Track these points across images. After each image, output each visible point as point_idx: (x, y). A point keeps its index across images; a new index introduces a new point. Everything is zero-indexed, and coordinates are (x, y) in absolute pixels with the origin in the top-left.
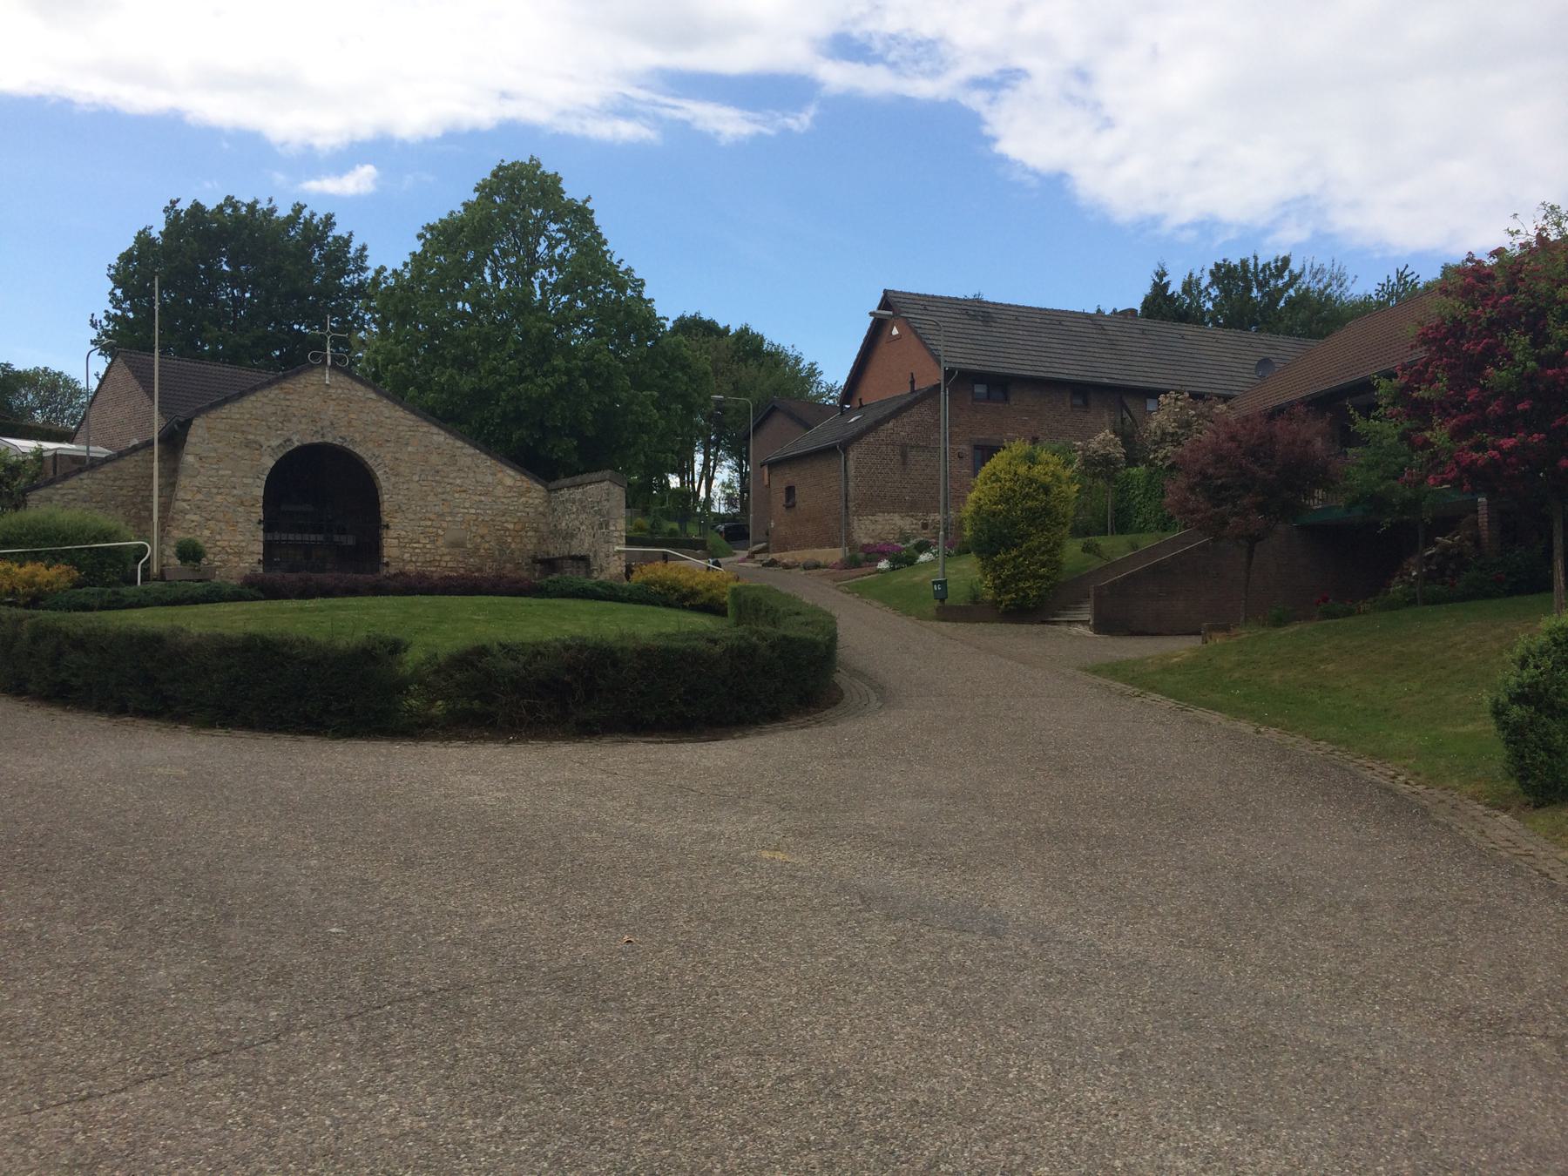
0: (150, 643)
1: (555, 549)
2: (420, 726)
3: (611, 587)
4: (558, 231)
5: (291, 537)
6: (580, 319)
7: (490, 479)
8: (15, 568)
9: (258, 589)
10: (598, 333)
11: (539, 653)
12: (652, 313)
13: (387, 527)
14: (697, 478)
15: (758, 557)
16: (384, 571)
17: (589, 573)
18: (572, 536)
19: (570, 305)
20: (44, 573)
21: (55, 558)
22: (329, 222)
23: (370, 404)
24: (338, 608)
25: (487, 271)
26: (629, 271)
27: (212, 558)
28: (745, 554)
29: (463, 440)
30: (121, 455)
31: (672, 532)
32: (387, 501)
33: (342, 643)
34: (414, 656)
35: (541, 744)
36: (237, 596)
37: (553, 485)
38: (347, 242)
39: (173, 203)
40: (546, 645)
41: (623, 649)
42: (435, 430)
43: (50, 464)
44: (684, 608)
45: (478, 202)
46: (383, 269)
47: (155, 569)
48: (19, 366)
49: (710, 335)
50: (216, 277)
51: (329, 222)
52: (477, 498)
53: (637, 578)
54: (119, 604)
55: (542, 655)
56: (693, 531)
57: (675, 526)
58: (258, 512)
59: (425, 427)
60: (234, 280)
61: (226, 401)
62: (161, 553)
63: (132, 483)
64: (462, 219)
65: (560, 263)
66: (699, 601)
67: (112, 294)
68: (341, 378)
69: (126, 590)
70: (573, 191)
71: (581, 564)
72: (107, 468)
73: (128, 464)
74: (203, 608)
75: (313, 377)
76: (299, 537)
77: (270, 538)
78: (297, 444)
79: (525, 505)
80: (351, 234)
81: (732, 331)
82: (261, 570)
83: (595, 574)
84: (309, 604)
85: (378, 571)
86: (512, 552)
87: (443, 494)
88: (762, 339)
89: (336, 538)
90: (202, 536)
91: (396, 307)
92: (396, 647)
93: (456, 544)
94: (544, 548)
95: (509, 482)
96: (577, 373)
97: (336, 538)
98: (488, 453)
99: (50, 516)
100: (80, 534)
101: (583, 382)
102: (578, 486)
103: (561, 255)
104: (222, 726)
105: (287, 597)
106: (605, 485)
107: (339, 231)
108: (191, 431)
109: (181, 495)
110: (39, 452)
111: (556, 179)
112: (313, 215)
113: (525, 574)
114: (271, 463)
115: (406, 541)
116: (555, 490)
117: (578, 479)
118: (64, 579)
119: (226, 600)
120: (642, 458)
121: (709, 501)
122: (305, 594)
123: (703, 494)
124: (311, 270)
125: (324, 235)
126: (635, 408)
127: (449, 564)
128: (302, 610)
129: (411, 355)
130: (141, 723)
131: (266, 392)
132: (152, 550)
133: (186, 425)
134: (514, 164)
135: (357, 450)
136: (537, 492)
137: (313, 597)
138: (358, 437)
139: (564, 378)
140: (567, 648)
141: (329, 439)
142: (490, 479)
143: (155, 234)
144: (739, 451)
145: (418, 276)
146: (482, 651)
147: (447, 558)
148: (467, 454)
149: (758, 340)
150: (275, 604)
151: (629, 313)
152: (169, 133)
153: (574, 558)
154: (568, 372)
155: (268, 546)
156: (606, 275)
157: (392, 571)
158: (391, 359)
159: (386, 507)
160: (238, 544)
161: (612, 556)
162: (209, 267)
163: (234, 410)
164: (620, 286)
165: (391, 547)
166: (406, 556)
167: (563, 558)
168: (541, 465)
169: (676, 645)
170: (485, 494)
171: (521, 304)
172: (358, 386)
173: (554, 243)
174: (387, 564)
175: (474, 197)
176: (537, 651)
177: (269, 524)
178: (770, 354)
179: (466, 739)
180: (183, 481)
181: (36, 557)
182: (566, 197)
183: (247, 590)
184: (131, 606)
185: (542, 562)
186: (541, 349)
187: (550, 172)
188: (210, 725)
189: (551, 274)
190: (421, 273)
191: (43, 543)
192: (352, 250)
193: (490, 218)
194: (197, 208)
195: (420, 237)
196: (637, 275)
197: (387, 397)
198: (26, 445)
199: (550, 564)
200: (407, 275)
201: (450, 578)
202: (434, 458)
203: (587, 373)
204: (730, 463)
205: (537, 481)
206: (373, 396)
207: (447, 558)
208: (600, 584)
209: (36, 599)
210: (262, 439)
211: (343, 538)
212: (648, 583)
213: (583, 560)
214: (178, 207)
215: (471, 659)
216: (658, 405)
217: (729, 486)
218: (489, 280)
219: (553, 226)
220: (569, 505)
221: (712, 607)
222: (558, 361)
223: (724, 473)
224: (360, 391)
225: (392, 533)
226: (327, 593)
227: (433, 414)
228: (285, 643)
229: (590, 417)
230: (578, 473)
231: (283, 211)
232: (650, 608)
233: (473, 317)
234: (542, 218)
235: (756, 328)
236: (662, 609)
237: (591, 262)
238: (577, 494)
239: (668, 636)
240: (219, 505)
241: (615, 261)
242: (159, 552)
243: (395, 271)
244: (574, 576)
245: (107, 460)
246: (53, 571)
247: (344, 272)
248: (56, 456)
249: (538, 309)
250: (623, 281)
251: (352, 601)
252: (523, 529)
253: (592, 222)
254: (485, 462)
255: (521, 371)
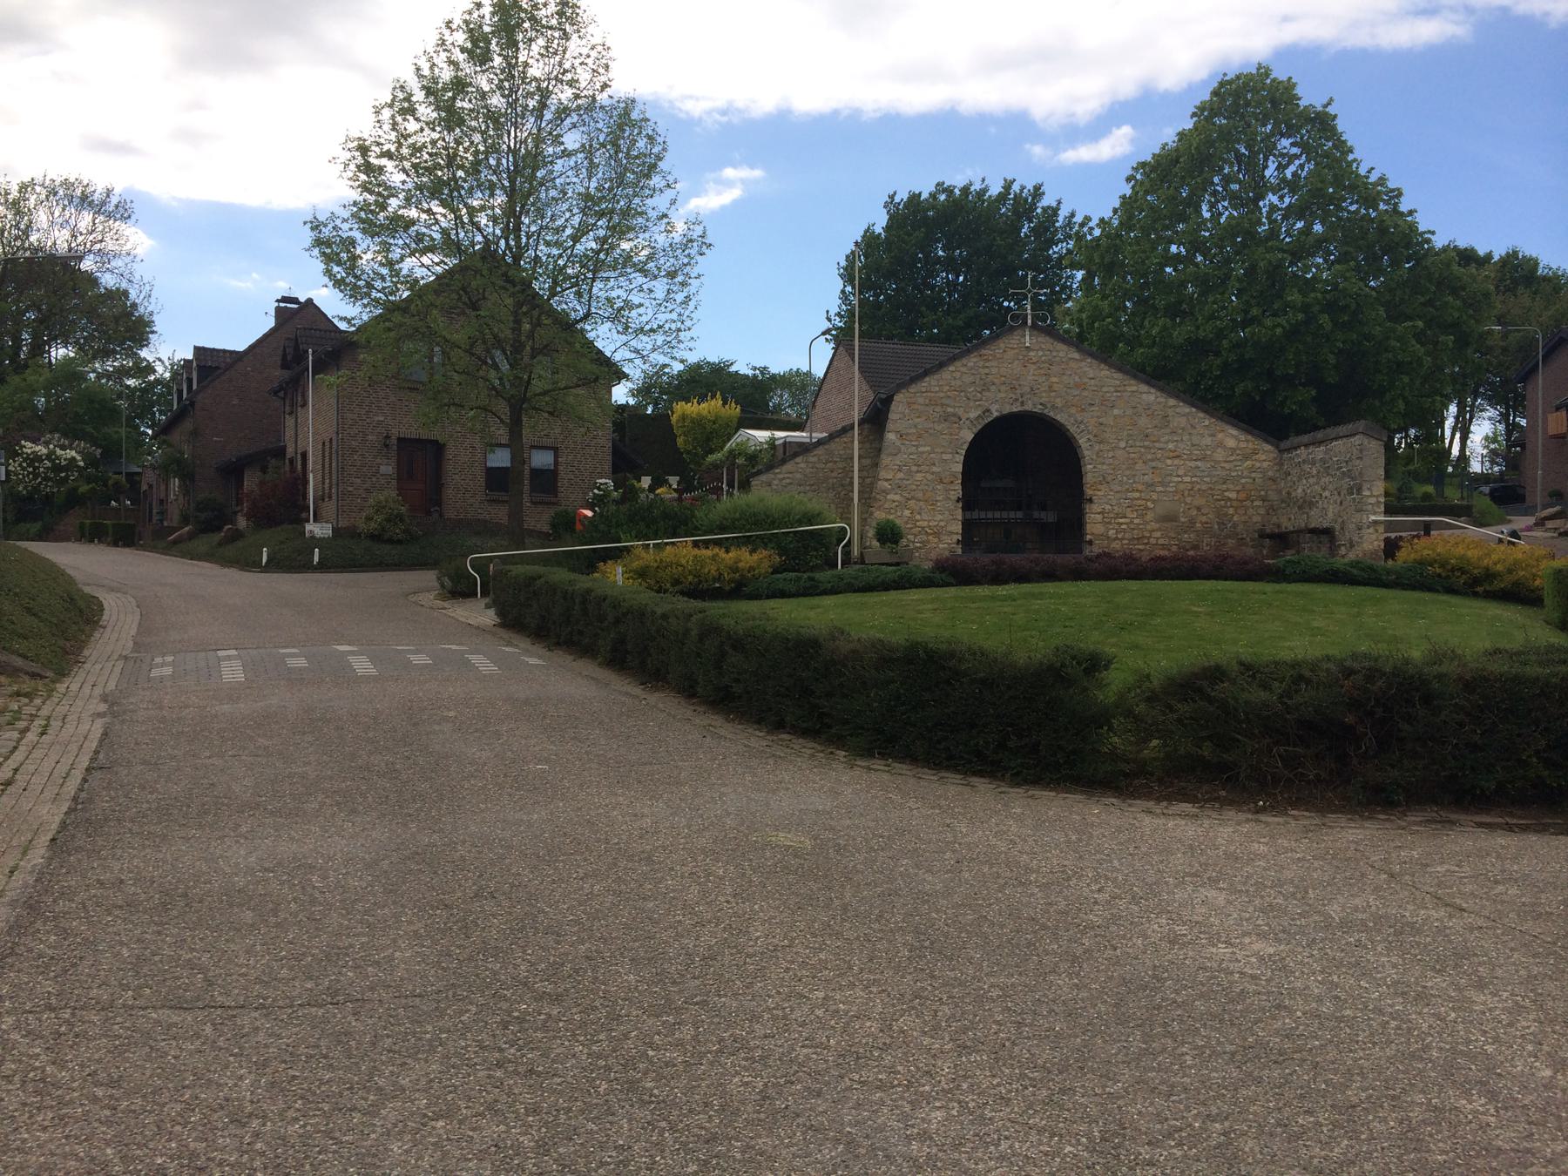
0: (804, 648)
1: (1289, 521)
2: (1126, 775)
3: (1371, 568)
4: (1292, 145)
5: (990, 515)
6: (1320, 243)
7: (1208, 441)
8: (722, 554)
9: (952, 573)
10: (1343, 258)
11: (1301, 678)
12: (1413, 227)
13: (1091, 501)
14: (1448, 433)
15: (1550, 524)
16: (1087, 551)
17: (1333, 548)
18: (1311, 505)
19: (1307, 230)
20: (746, 558)
21: (764, 542)
22: (1038, 192)
23: (1073, 365)
24: (1033, 596)
25: (1205, 208)
26: (1382, 180)
27: (911, 540)
28: (1531, 520)
29: (1177, 397)
30: (832, 437)
31: (1426, 497)
32: (1091, 472)
33: (1020, 657)
34: (1116, 679)
35: (1308, 819)
36: (927, 582)
37: (1284, 444)
38: (1054, 211)
39: (892, 197)
40: (1314, 666)
41: (1440, 677)
42: (1144, 388)
43: (781, 450)
44: (1476, 595)
45: (1196, 128)
46: (1088, 219)
47: (856, 552)
48: (774, 370)
49: (1467, 264)
50: (932, 263)
51: (1038, 192)
52: (1193, 464)
53: (1404, 555)
54: (812, 590)
55: (1308, 682)
56: (1453, 495)
57: (1430, 489)
58: (957, 490)
59: (1134, 386)
60: (950, 264)
61: (926, 373)
62: (862, 537)
63: (840, 465)
64: (1177, 150)
65: (1293, 185)
66: (1499, 585)
67: (843, 292)
68: (1043, 339)
69: (824, 576)
70: (1310, 96)
71: (1324, 538)
72: (820, 451)
73: (836, 446)
74: (893, 595)
75: (1012, 341)
76: (997, 515)
77: (968, 516)
78: (996, 414)
79: (1252, 469)
80: (1059, 203)
81: (1496, 258)
82: (959, 551)
83: (1343, 551)
84: (1002, 590)
85: (1080, 551)
86: (1235, 526)
87: (1155, 461)
88: (1536, 263)
89: (1036, 514)
90: (900, 518)
91: (1102, 257)
92: (1094, 664)
93: (1169, 518)
94: (1274, 519)
95: (1231, 443)
96: (1316, 309)
97: (1036, 514)
98: (1206, 412)
99: (761, 500)
100: (785, 518)
101: (1324, 319)
102: (1320, 443)
103: (1294, 174)
104: (883, 756)
105: (979, 583)
106: (1357, 440)
107: (1047, 201)
108: (893, 407)
109: (883, 474)
110: (773, 439)
111: (1289, 86)
112: (1023, 188)
113: (1250, 551)
114: (969, 436)
115: (1110, 518)
116: (1288, 450)
117: (1320, 435)
118: (766, 564)
119: (917, 587)
120: (1401, 405)
121: (1463, 459)
122: (997, 579)
123: (1455, 451)
124: (1019, 243)
125: (1033, 207)
126: (1393, 343)
127: (1159, 541)
128: (993, 598)
129: (1117, 309)
130: (798, 743)
131: (964, 361)
132: (853, 533)
133: (888, 401)
134: (1238, 77)
135: (1058, 418)
136: (1265, 453)
137: (1006, 582)
138: (1059, 402)
139: (1300, 316)
140: (1349, 673)
141: (1029, 407)
142: (1208, 441)
143: (878, 229)
144: (1509, 399)
145: (1127, 223)
146: (1215, 674)
147: (1158, 534)
148: (1182, 413)
149: (1533, 263)
150: (966, 591)
151: (1383, 230)
152: (892, 128)
153: (1314, 531)
154: (1305, 308)
155: (967, 525)
156: (1352, 188)
157: (1096, 550)
158: (1097, 316)
159: (1089, 478)
160: (934, 520)
161: (1367, 529)
162: (927, 256)
163: (934, 383)
164: (1370, 200)
165: (1095, 524)
166: (1111, 533)
167: (1299, 532)
168: (1268, 419)
169: (1533, 671)
170: (1203, 459)
171: (1243, 234)
172: (1061, 346)
173: (1286, 161)
174: (1090, 543)
175: (1189, 124)
176: (1299, 675)
177: (968, 502)
178: (1545, 279)
179: (1192, 800)
180: (885, 460)
181: (738, 543)
182: (1303, 103)
183: (937, 575)
184: (825, 593)
185: (1271, 536)
186: (1269, 286)
187: (1283, 77)
188: (868, 753)
189: (1281, 198)
190: (1131, 217)
191: (752, 528)
192: (1061, 219)
193: (1211, 143)
194: (914, 198)
195: (1128, 180)
196: (1391, 185)
197: (1092, 355)
198: (762, 435)
199: (1282, 540)
200: (1116, 222)
201: (1163, 558)
202: (1143, 421)
203: (1331, 307)
204: (1491, 412)
205: (1268, 442)
206: (1076, 355)
207: (1158, 534)
208: (1355, 564)
209: (740, 588)
210: (960, 412)
211: (1043, 515)
212: (1422, 563)
213: (1327, 532)
214: (897, 199)
215: (1196, 686)
216: (1419, 336)
217: (1494, 440)
218: (1207, 215)
219: (1285, 142)
220: (1307, 467)
221: (1519, 594)
222: (1294, 297)
223: (1482, 429)
224: (1063, 351)
225: (1096, 507)
226: (1021, 577)
227: (1143, 371)
228: (952, 655)
229: (1332, 359)
230: (1316, 428)
231: (995, 190)
232: (1427, 596)
233: (1188, 259)
234: (1272, 134)
235: (1528, 249)
236: (1445, 597)
237: (1333, 174)
238: (1319, 452)
239: (1512, 655)
240: (920, 489)
241: (1362, 172)
242: (857, 532)
243: (1102, 220)
244: (1313, 553)
245: (820, 442)
246: (755, 557)
247: (1052, 242)
248: (786, 444)
249: (1267, 239)
250: (1372, 193)
251: (1050, 587)
252: (1247, 499)
253: (1334, 128)
254: (1203, 421)
255: (1246, 312)
